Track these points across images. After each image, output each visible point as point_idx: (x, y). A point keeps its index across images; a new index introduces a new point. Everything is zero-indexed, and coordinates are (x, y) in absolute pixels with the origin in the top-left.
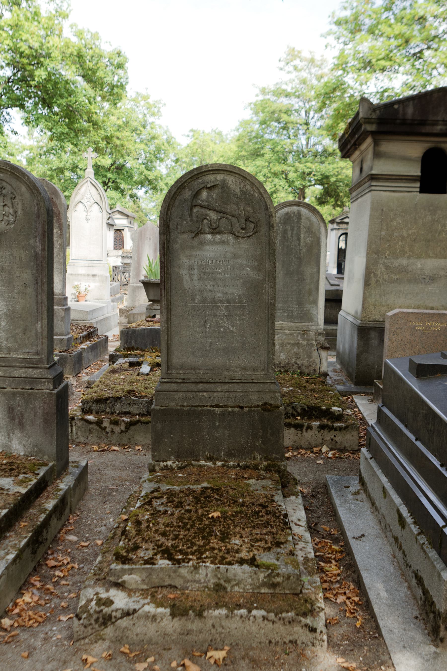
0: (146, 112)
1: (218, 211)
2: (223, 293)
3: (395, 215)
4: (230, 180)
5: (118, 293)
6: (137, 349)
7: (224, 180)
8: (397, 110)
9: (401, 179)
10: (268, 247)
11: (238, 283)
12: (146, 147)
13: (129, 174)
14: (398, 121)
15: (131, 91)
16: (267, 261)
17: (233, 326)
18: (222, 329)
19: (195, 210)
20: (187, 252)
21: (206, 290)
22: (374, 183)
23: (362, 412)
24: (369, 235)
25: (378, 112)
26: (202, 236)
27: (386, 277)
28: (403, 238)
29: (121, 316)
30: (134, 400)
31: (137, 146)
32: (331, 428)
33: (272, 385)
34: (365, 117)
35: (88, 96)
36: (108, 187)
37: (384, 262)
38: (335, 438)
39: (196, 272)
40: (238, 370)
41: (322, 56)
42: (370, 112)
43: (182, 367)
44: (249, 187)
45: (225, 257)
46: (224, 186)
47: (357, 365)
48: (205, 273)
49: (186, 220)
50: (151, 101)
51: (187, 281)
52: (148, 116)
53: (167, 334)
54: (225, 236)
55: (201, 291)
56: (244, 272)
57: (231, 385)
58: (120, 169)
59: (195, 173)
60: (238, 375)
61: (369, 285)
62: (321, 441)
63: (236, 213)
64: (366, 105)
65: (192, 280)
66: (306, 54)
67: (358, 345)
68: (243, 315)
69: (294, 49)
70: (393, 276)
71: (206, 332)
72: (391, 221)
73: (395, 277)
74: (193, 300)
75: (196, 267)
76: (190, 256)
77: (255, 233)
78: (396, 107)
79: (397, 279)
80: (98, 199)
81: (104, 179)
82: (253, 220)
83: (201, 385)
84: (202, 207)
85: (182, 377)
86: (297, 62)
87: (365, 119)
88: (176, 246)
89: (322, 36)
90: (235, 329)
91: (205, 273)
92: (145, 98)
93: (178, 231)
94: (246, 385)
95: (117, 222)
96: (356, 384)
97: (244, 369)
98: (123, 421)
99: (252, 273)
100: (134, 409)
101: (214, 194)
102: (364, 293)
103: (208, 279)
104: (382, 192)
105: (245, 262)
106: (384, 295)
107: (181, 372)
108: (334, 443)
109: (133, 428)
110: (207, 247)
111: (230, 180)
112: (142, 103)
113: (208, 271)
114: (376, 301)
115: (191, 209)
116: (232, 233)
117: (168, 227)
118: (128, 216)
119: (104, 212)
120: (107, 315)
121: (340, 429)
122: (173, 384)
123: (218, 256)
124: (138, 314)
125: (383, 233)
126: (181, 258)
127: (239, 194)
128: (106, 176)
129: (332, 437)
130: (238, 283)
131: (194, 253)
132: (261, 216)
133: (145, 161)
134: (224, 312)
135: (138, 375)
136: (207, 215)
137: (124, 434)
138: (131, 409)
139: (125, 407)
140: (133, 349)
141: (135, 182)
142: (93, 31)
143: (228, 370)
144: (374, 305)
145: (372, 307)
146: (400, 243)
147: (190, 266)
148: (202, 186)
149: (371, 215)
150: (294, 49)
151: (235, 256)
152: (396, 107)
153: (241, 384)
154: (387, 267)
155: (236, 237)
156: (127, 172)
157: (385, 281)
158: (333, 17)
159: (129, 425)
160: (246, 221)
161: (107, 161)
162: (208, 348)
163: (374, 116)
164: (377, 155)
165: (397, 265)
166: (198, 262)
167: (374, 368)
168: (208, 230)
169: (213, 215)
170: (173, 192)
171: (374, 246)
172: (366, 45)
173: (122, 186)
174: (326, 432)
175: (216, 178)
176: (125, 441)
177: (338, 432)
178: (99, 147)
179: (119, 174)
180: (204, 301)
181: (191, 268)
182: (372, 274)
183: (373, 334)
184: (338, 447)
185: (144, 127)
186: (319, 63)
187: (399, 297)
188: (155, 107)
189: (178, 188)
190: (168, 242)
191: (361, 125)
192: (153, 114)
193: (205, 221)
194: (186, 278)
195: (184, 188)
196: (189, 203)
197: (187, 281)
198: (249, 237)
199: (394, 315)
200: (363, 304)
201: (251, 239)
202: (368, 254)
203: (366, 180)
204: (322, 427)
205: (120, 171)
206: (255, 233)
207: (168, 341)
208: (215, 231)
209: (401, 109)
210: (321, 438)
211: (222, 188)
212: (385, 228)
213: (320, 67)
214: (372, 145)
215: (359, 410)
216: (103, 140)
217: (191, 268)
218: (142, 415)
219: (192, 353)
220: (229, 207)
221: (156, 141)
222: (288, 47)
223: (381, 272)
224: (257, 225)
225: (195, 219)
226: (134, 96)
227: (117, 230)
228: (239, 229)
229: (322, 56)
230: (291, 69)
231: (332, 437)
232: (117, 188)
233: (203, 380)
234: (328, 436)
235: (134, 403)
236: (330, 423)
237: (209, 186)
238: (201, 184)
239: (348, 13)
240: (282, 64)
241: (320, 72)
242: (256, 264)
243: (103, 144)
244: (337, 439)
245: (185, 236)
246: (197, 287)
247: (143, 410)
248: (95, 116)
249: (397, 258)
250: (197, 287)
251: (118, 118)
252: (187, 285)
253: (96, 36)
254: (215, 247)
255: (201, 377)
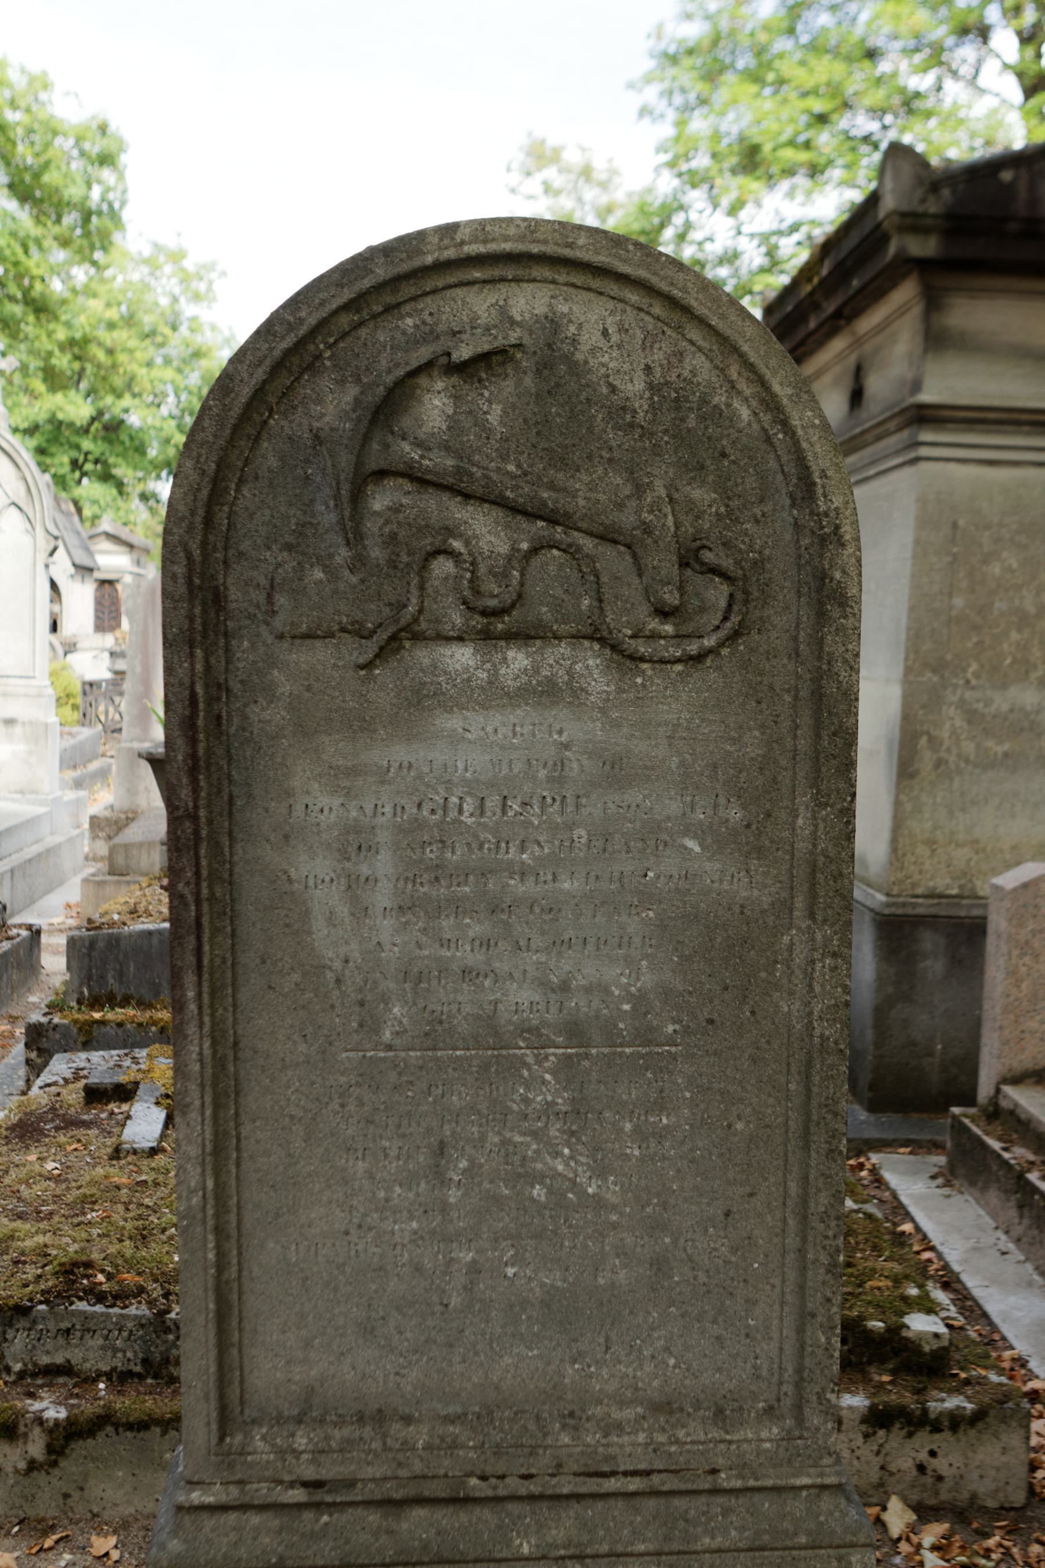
0: (177, 290)
1: (514, 509)
2: (543, 984)
3: (997, 540)
4: (592, 322)
5: (95, 756)
6: (125, 1002)
7: (553, 324)
8: (1010, 187)
9: (1018, 423)
10: (806, 720)
11: (633, 926)
12: (179, 378)
13: (137, 443)
14: (1013, 227)
15: (136, 235)
16: (804, 799)
17: (601, 1172)
18: (538, 1192)
19: (381, 500)
20: (334, 748)
21: (444, 970)
22: (926, 436)
23: (936, 1242)
24: (912, 609)
25: (946, 192)
26: (423, 655)
27: (969, 747)
28: (1023, 621)
29: (94, 837)
30: (86, 1316)
31: (156, 373)
32: (918, 1422)
33: (827, 1503)
34: (905, 207)
35: (22, 234)
36: (84, 474)
37: (962, 700)
38: (935, 1463)
39: (384, 864)
40: (628, 1413)
41: (610, 160)
42: (919, 193)
43: (308, 1410)
44: (699, 366)
45: (558, 780)
46: (551, 356)
47: (877, 1045)
48: (438, 872)
49: (325, 562)
50: (189, 264)
51: (331, 920)
52: (182, 300)
53: (219, 1231)
54: (557, 657)
55: (415, 977)
56: (671, 864)
57: (591, 1511)
58: (113, 429)
59: (382, 272)
60: (631, 1447)
61: (912, 776)
62: (875, 1475)
63: (627, 519)
64: (907, 168)
65: (361, 912)
66: (572, 157)
67: (881, 980)
68: (660, 1106)
69: (543, 142)
70: (990, 744)
71: (445, 1208)
72: (985, 561)
73: (1000, 749)
74: (370, 1025)
75: (383, 837)
76: (354, 772)
77: (735, 635)
78: (1006, 176)
79: (1006, 755)
80: (17, 491)
81: (74, 454)
82: (727, 563)
83: (420, 1513)
84: (422, 480)
85: (309, 1473)
86: (551, 173)
87: (904, 215)
88: (268, 715)
89: (631, 86)
90: (612, 1190)
91: (438, 872)
92: (177, 256)
93: (279, 623)
94: (679, 1503)
95: (102, 560)
96: (874, 1107)
97: (665, 1408)
98: (40, 1421)
99: (712, 867)
100: (88, 1354)
101: (495, 405)
102: (897, 804)
103: (458, 907)
104: (952, 466)
105: (674, 808)
106: (963, 810)
107: (301, 1442)
108: (929, 1480)
109: (80, 1448)
110: (453, 722)
111: (592, 322)
112: (168, 269)
113: (454, 857)
114: (936, 827)
115: (357, 497)
116: (597, 635)
117: (217, 599)
118: (131, 546)
119: (40, 531)
120: (50, 841)
121: (955, 1422)
122: (255, 1519)
123: (507, 775)
124: (141, 845)
125: (959, 602)
126: (296, 783)
127: (641, 405)
128: (78, 447)
129: (923, 1456)
130: (633, 926)
131: (376, 755)
132: (770, 534)
133: (176, 412)
134: (549, 1092)
135: (117, 1154)
136: (450, 532)
137: (41, 1477)
138: (74, 1355)
139: (50, 1345)
140: (112, 1001)
141: (151, 462)
142: (35, 68)
143: (572, 1420)
144: (931, 843)
145: (922, 851)
146: (1014, 635)
147: (355, 828)
148: (423, 354)
149: (917, 542)
150: (543, 142)
151: (615, 771)
152: (1006, 176)
153: (652, 1503)
154: (972, 717)
155: (623, 657)
156: (131, 438)
157: (967, 761)
158: (659, 37)
159: (65, 1437)
160: (684, 564)
161: (77, 408)
162: (455, 1301)
163: (933, 207)
164: (936, 340)
165: (1005, 707)
166: (398, 809)
167: (931, 1054)
168: (457, 618)
169: (487, 533)
170: (245, 393)
171: (927, 646)
172: (743, 112)
173: (117, 472)
174: (894, 1439)
175: (503, 311)
176: (46, 1506)
177: (947, 1434)
178: (53, 368)
179: (110, 442)
180: (434, 1033)
181: (355, 842)
182: (923, 741)
183: (929, 941)
184: (944, 1496)
185: (174, 328)
186: (604, 177)
187: (1013, 816)
188: (201, 279)
189: (277, 367)
190: (218, 689)
191: (885, 239)
192: (197, 297)
193: (442, 567)
194: (327, 898)
195: (313, 366)
196: (345, 460)
197: (331, 920)
198: (698, 658)
199: (1025, 886)
200: (894, 840)
201: (710, 675)
202: (908, 671)
203: (892, 425)
204: (878, 1419)
205: (113, 436)
206: (735, 635)
207: (221, 1266)
208: (496, 623)
209: (1023, 185)
210: (877, 1461)
211: (544, 367)
212: (964, 584)
213: (604, 185)
214: (917, 310)
215: (918, 1229)
216: (62, 347)
217: (355, 842)
218: (120, 1378)
219: (367, 1331)
220: (579, 483)
221: (204, 363)
222: (530, 134)
223: (953, 732)
224: (744, 586)
225: (376, 553)
226: (147, 251)
227: (103, 582)
228: (643, 611)
229: (610, 160)
230: (539, 190)
231: (923, 1456)
232: (106, 477)
233: (429, 1489)
234: (906, 1452)
235: (88, 1326)
236: (908, 1400)
237: (463, 353)
238: (418, 342)
239: (694, 31)
240: (515, 178)
241: (604, 200)
242: (735, 814)
243: (62, 361)
244: (940, 1465)
245: (319, 655)
246: (390, 954)
247: (129, 1357)
248: (38, 287)
249: (1004, 686)
250: (390, 954)
251: (108, 305)
252: (331, 940)
253: (41, 83)
254: (496, 719)
255: (418, 1467)
